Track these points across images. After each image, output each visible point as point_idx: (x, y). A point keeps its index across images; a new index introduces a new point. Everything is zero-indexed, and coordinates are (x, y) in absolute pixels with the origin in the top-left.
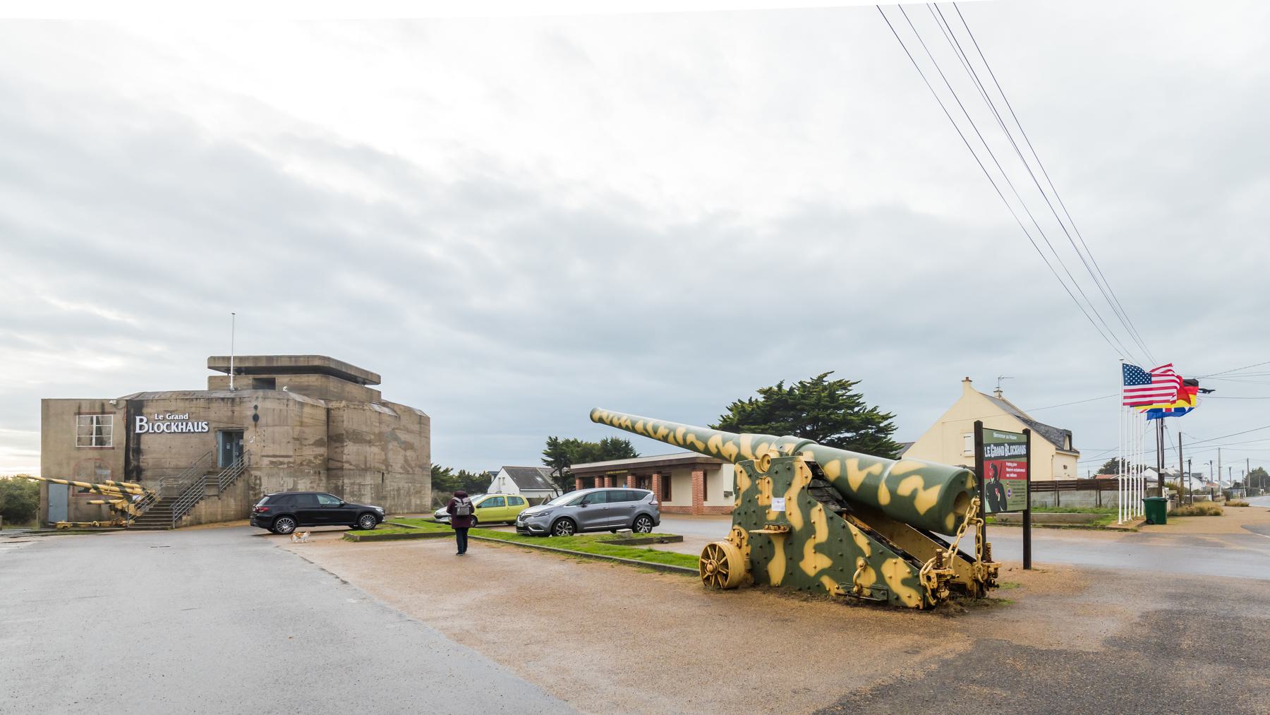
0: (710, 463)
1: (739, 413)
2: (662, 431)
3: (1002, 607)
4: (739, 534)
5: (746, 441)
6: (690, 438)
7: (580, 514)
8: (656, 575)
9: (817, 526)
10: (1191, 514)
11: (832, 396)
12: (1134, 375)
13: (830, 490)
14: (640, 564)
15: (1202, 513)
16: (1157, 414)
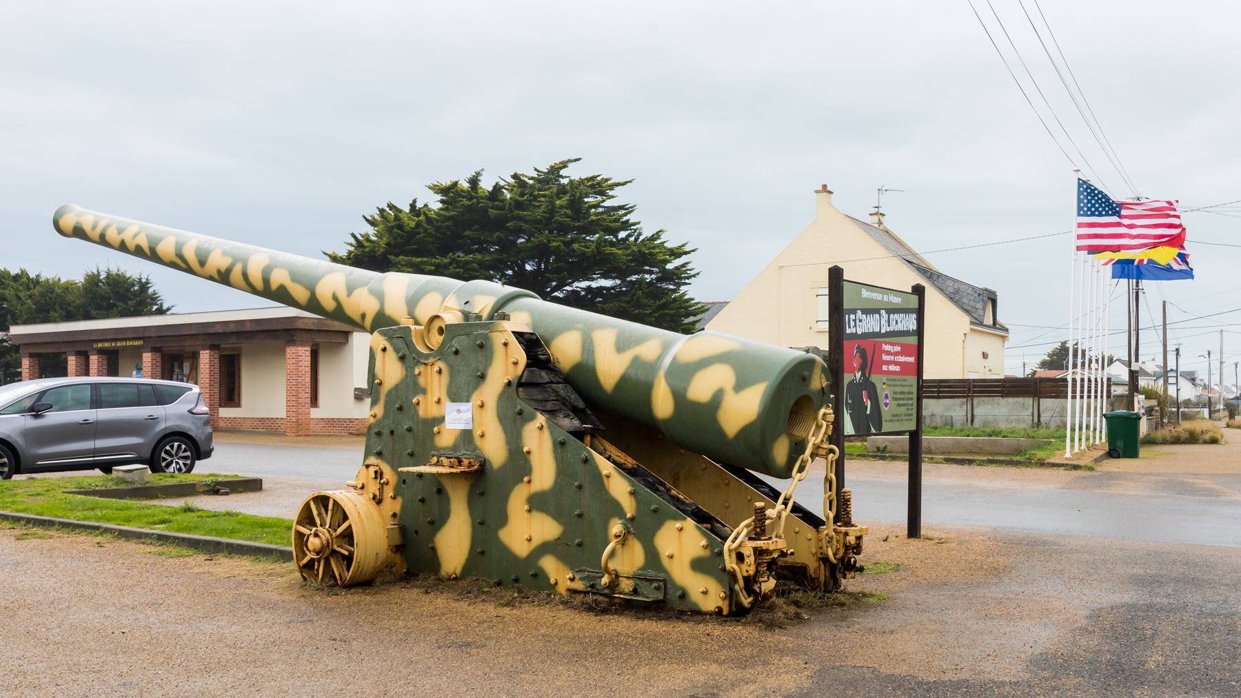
0: (326, 330)
1: (390, 230)
2: (217, 261)
3: (868, 607)
4: (379, 475)
5: (396, 288)
6: (279, 278)
7: (29, 434)
8: (197, 562)
9: (535, 460)
10: (1177, 441)
11: (577, 207)
12: (1094, 201)
13: (561, 389)
14: (162, 538)
15: (1192, 439)
16: (1125, 269)
